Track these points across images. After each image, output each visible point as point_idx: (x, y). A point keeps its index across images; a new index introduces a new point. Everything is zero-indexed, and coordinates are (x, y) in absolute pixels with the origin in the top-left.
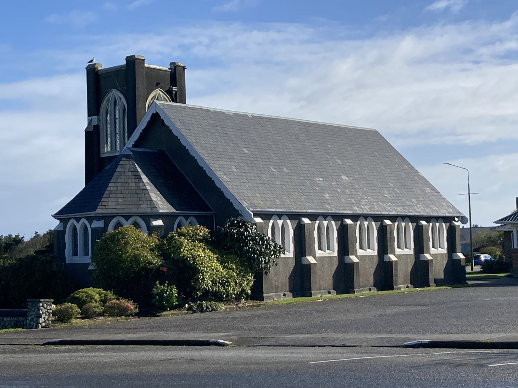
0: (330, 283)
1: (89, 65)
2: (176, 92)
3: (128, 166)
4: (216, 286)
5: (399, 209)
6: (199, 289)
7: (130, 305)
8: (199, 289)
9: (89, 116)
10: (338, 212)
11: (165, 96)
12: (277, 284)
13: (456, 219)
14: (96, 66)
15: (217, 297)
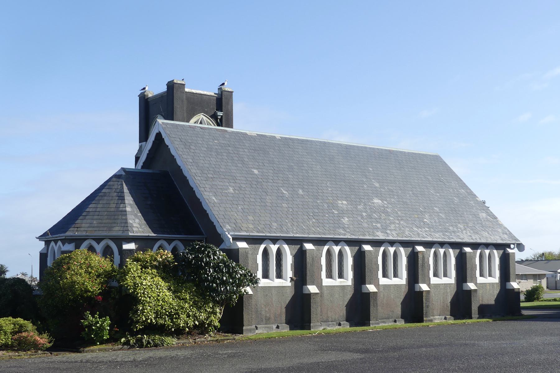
0: (342, 314)
3: (116, 187)
4: (161, 317)
5: (437, 235)
6: (138, 322)
7: (43, 340)
8: (138, 322)
9: (140, 142)
10: (353, 237)
12: (268, 315)
13: (512, 246)
14: (146, 94)
15: (162, 330)
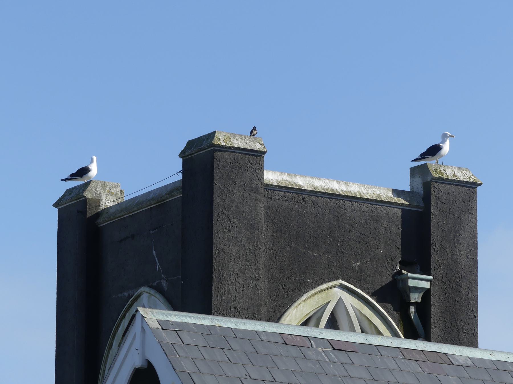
1: (69, 192)
2: (427, 294)
11: (368, 312)
14: (88, 194)
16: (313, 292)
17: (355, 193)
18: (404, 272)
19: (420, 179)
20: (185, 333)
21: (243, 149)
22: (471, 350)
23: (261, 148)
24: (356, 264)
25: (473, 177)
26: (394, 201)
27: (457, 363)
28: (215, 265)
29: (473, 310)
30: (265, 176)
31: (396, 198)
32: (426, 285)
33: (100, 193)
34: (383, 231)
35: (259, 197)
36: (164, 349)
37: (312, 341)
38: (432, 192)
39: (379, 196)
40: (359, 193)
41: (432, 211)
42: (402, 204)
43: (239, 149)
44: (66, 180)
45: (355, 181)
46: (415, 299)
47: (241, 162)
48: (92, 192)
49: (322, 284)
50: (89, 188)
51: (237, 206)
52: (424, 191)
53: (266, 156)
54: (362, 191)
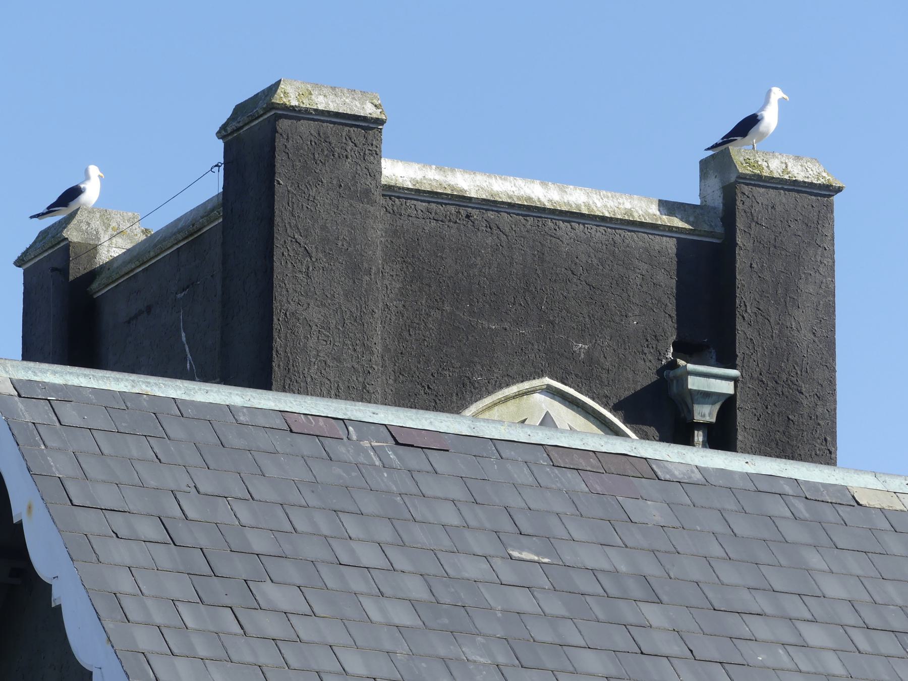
1: (43, 234)
2: (728, 405)
14: (72, 234)
16: (488, 401)
17: (578, 206)
18: (681, 362)
19: (717, 180)
20: (68, 404)
21: (337, 115)
22: (704, 454)
23: (375, 113)
24: (581, 347)
25: (824, 174)
26: (659, 223)
27: (668, 477)
28: (278, 343)
29: (826, 440)
30: (385, 172)
31: (664, 217)
32: (727, 388)
33: (97, 232)
34: (638, 281)
35: (372, 209)
36: (16, 433)
37: (351, 429)
38: (739, 203)
39: (629, 212)
40: (588, 206)
41: (739, 240)
42: (678, 228)
43: (329, 113)
44: (38, 216)
45: (580, 182)
46: (704, 416)
47: (334, 141)
48: (80, 230)
49: (508, 385)
50: (75, 221)
51: (324, 228)
52: (724, 205)
53: (385, 128)
54: (594, 203)
